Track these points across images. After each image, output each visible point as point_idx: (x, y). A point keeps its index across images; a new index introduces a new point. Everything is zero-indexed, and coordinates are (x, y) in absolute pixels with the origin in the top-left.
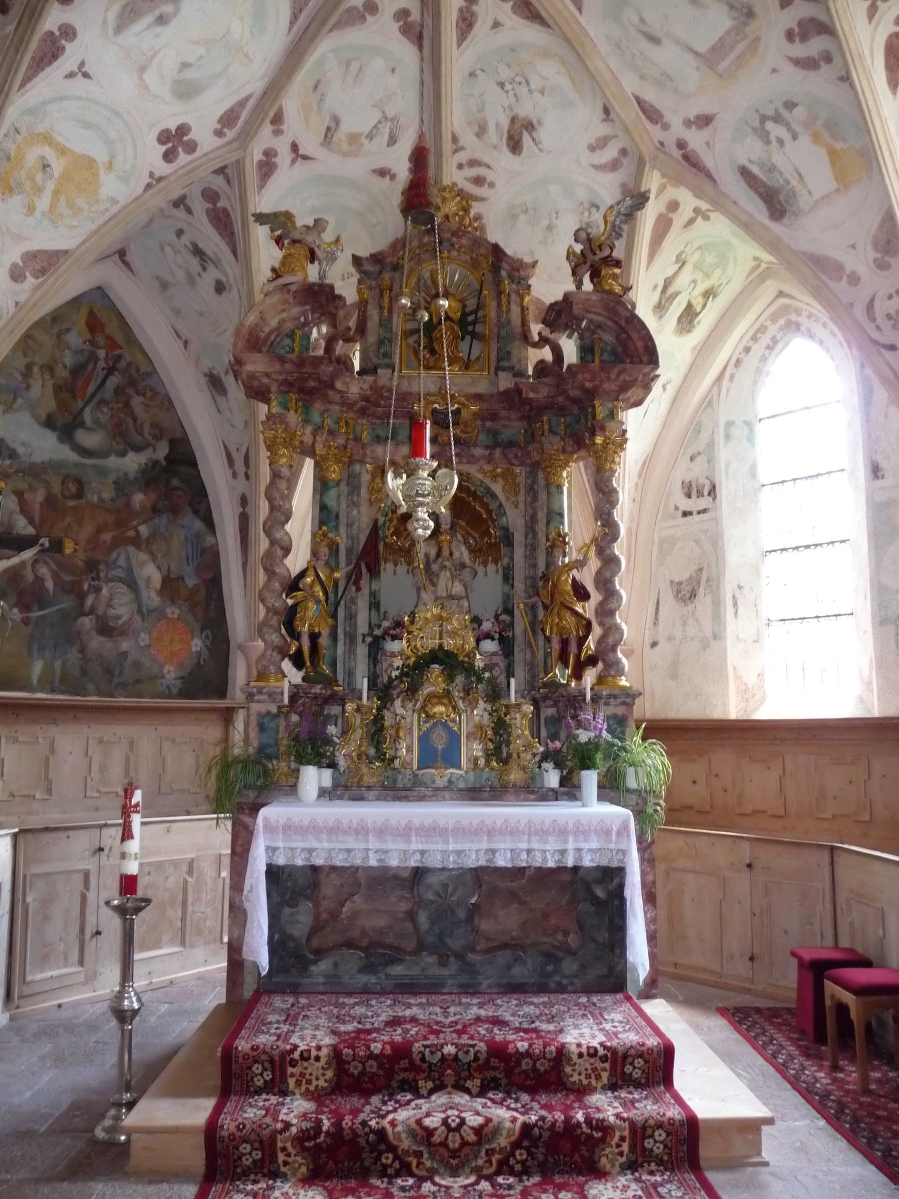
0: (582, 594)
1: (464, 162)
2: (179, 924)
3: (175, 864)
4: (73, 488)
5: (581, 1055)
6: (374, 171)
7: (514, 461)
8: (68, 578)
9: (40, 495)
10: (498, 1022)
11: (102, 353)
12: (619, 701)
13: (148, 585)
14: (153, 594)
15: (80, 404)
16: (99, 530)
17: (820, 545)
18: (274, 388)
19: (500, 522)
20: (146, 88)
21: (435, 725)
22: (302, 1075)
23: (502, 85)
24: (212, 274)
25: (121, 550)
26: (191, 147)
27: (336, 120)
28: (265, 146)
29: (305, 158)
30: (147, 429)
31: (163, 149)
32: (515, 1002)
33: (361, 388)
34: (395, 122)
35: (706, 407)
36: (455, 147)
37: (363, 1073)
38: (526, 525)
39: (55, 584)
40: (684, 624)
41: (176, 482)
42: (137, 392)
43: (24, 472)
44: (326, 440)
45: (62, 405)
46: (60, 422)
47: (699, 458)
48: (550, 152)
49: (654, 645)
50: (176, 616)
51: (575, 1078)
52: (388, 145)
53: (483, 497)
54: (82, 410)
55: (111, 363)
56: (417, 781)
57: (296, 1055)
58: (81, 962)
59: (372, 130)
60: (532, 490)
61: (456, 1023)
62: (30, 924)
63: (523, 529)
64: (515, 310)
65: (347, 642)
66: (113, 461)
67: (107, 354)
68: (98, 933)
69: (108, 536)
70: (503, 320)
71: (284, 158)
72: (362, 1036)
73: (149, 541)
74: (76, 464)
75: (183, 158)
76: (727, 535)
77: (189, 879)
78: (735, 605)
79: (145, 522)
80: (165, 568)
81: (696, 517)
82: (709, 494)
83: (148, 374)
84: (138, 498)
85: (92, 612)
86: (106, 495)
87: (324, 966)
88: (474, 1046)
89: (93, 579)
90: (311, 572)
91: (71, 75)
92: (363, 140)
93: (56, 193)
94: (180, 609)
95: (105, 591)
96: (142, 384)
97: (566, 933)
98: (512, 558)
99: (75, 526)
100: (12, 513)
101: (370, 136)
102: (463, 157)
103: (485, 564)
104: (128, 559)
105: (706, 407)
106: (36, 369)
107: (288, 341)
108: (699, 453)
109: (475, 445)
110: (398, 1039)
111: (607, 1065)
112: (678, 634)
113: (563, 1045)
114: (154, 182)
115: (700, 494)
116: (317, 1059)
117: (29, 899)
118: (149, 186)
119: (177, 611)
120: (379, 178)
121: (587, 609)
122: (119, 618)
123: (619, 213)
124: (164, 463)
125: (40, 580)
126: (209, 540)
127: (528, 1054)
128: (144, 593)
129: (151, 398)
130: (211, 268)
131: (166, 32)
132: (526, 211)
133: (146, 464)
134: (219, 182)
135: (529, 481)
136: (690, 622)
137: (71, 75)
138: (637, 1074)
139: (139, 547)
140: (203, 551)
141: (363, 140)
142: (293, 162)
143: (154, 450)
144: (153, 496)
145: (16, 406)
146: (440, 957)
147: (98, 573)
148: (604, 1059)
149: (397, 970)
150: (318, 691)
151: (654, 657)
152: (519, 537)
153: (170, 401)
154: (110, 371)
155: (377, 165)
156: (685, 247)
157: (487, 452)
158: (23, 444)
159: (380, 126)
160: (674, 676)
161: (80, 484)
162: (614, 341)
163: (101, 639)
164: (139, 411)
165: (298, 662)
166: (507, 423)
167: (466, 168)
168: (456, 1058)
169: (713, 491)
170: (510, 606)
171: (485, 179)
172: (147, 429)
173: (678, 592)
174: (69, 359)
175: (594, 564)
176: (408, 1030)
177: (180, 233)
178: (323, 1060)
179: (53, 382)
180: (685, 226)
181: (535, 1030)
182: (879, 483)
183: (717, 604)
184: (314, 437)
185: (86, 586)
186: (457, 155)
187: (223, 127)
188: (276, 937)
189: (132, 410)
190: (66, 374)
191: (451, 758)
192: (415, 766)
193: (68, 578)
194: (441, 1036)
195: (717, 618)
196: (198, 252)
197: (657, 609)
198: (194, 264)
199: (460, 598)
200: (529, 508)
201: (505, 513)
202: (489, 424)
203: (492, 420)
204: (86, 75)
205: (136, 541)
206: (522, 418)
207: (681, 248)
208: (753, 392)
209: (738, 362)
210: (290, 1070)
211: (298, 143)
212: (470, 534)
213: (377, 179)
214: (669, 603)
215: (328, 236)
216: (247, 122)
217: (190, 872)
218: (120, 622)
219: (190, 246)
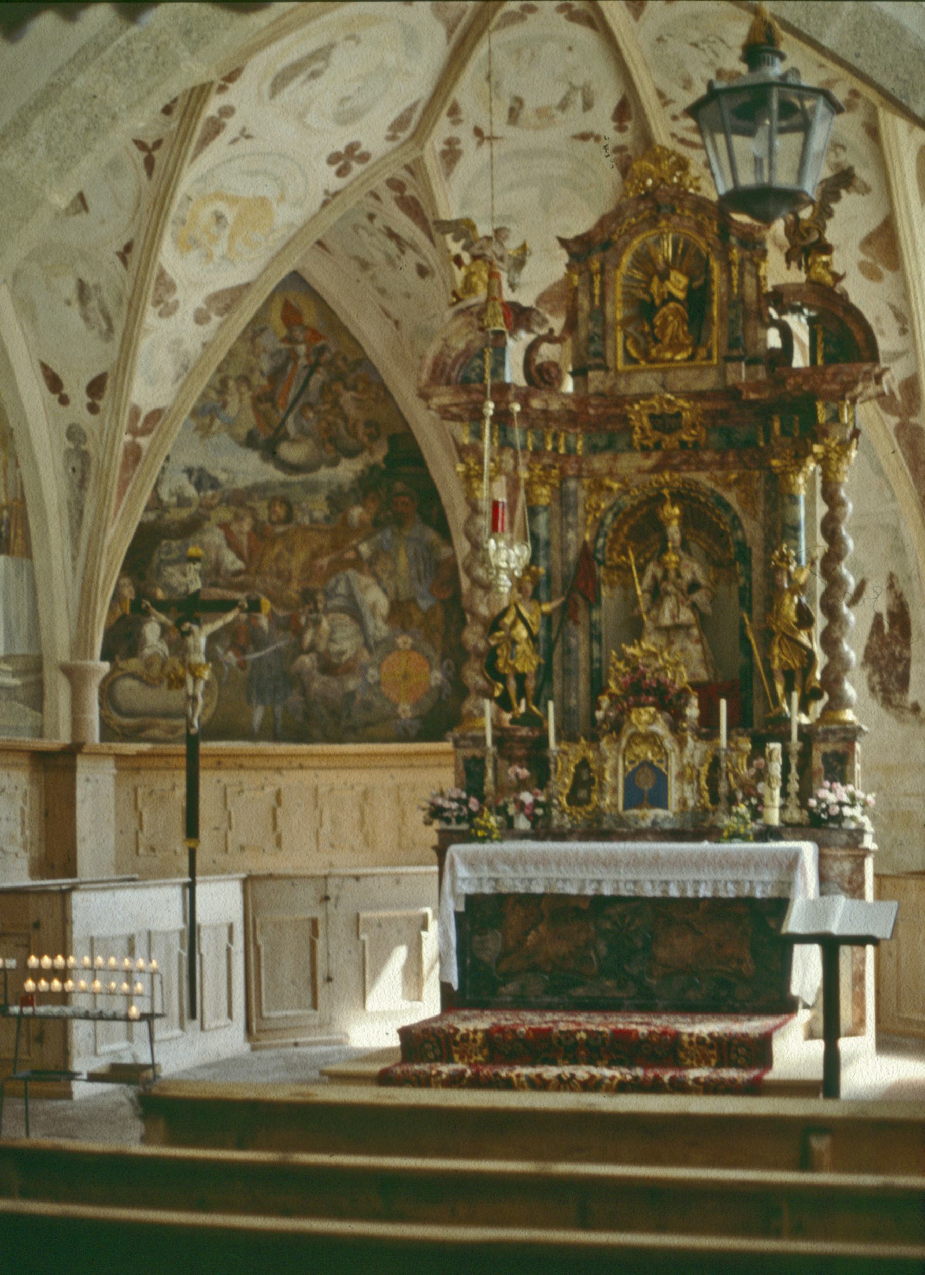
4: (280, 511)
5: (691, 1043)
6: (575, 137)
8: (281, 613)
9: (246, 525)
11: (302, 349)
13: (373, 614)
14: (380, 623)
15: (282, 412)
16: (314, 556)
20: (309, 127)
23: (696, 45)
24: (410, 260)
26: (364, 158)
30: (361, 430)
31: (334, 168)
39: (270, 622)
41: (399, 486)
42: (347, 388)
45: (261, 416)
46: (262, 438)
50: (408, 646)
54: (283, 422)
55: (313, 358)
57: (458, 1038)
62: (263, 964)
66: (324, 474)
67: (308, 349)
69: (324, 561)
71: (468, 143)
73: (372, 561)
74: (284, 484)
75: (357, 168)
80: (391, 592)
84: (356, 513)
86: (318, 515)
87: (511, 987)
89: (311, 612)
90: (513, 611)
91: (234, 141)
93: (232, 237)
95: (325, 624)
97: (740, 962)
98: (749, 578)
99: (286, 555)
100: (219, 548)
106: (231, 384)
111: (714, 1052)
114: (330, 198)
117: (260, 942)
118: (325, 204)
119: (410, 641)
122: (342, 653)
124: (383, 466)
126: (445, 552)
128: (370, 625)
130: (409, 252)
131: (319, 84)
133: (363, 471)
134: (403, 175)
137: (234, 141)
139: (360, 571)
141: (554, 111)
145: (214, 428)
147: (316, 603)
148: (711, 1047)
149: (580, 992)
154: (312, 369)
157: (718, 458)
158: (225, 470)
161: (288, 504)
163: (325, 678)
164: (351, 410)
172: (361, 430)
174: (266, 365)
175: (820, 586)
177: (371, 217)
178: (479, 1041)
179: (250, 393)
185: (303, 620)
187: (395, 131)
188: (468, 961)
189: (341, 408)
190: (264, 382)
191: (659, 799)
193: (281, 613)
196: (392, 235)
198: (392, 246)
202: (720, 422)
204: (248, 137)
205: (357, 563)
211: (481, 127)
213: (579, 143)
215: (512, 246)
218: (344, 658)
219: (384, 229)
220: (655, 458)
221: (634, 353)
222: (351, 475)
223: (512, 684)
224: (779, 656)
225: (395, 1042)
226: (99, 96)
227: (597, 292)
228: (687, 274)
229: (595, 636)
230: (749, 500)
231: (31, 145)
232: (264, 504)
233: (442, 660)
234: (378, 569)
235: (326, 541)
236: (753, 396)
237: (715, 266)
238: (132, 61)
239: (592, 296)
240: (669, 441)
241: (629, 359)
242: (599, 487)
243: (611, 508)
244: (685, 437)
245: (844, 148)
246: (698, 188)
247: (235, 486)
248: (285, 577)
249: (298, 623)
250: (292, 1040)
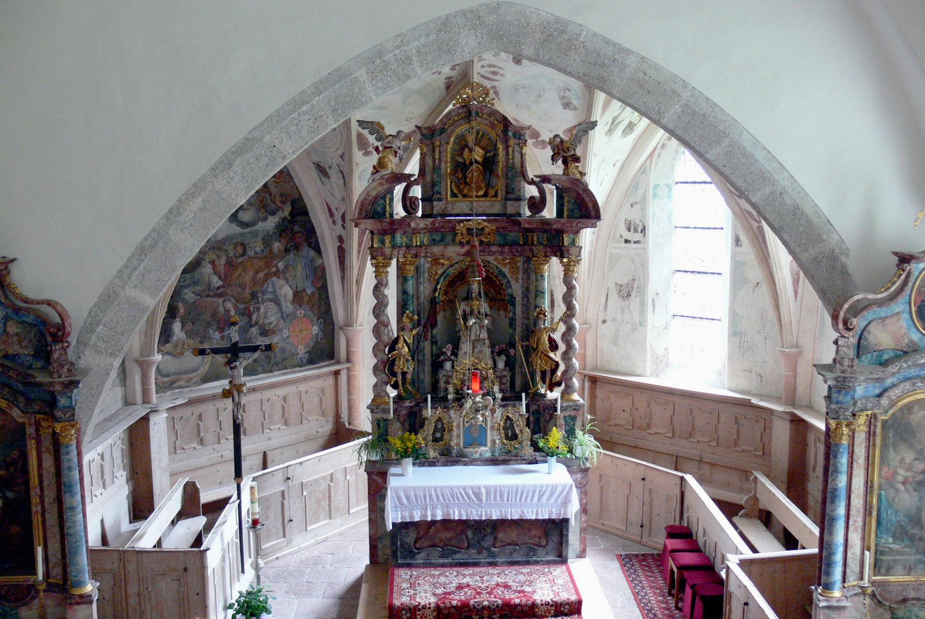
0: (554, 346)
2: (328, 508)
3: (324, 478)
4: (240, 250)
7: (516, 254)
9: (223, 261)
10: (506, 586)
14: (289, 304)
17: (706, 273)
22: (423, 614)
25: (269, 281)
30: (278, 198)
32: (514, 572)
35: (642, 173)
37: (449, 613)
38: (523, 293)
40: (623, 312)
43: (213, 248)
44: (405, 254)
47: (636, 206)
49: (604, 322)
51: (540, 613)
56: (462, 455)
57: (420, 607)
58: (284, 536)
60: (526, 271)
61: (487, 587)
64: (517, 156)
66: (260, 226)
68: (291, 520)
69: (261, 275)
70: (510, 165)
72: (447, 596)
74: (241, 234)
76: (651, 261)
77: (331, 484)
78: (654, 306)
81: (632, 244)
82: (641, 232)
84: (277, 246)
85: (256, 324)
86: (258, 249)
88: (496, 602)
89: (255, 303)
94: (305, 310)
95: (262, 309)
98: (514, 313)
99: (243, 274)
104: (274, 287)
105: (642, 173)
107: (382, 201)
108: (637, 203)
110: (463, 598)
112: (619, 317)
113: (535, 600)
115: (636, 231)
116: (429, 608)
119: (303, 312)
121: (556, 356)
122: (271, 323)
124: (289, 218)
125: (227, 311)
126: (319, 262)
127: (519, 605)
128: (284, 306)
132: (525, 87)
136: (627, 311)
138: (566, 611)
139: (279, 278)
140: (316, 269)
143: (283, 211)
146: (478, 550)
148: (552, 606)
149: (458, 556)
150: (408, 405)
151: (603, 329)
152: (519, 300)
153: (290, 175)
157: (499, 249)
160: (615, 344)
165: (395, 386)
168: (489, 607)
169: (643, 230)
173: (620, 291)
175: (562, 328)
176: (467, 592)
178: (432, 609)
181: (523, 592)
182: (738, 249)
183: (643, 304)
193: (241, 306)
194: (482, 595)
195: (643, 313)
197: (607, 300)
201: (511, 287)
205: (277, 274)
208: (672, 165)
209: (663, 146)
210: (418, 613)
214: (614, 296)
217: (331, 480)
218: (272, 326)
221: (455, 191)
222: (273, 225)
223: (400, 377)
224: (539, 364)
226: (277, 146)
227: (437, 157)
228: (483, 148)
229: (434, 343)
230: (515, 270)
231: (232, 174)
232: (232, 247)
233: (318, 320)
235: (262, 263)
236: (527, 226)
237: (500, 146)
238: (299, 126)
239: (434, 159)
241: (454, 195)
242: (436, 261)
243: (442, 274)
244: (483, 239)
245: (569, 90)
246: (493, 104)
247: (217, 239)
248: (243, 286)
249: (249, 311)
250: (275, 557)
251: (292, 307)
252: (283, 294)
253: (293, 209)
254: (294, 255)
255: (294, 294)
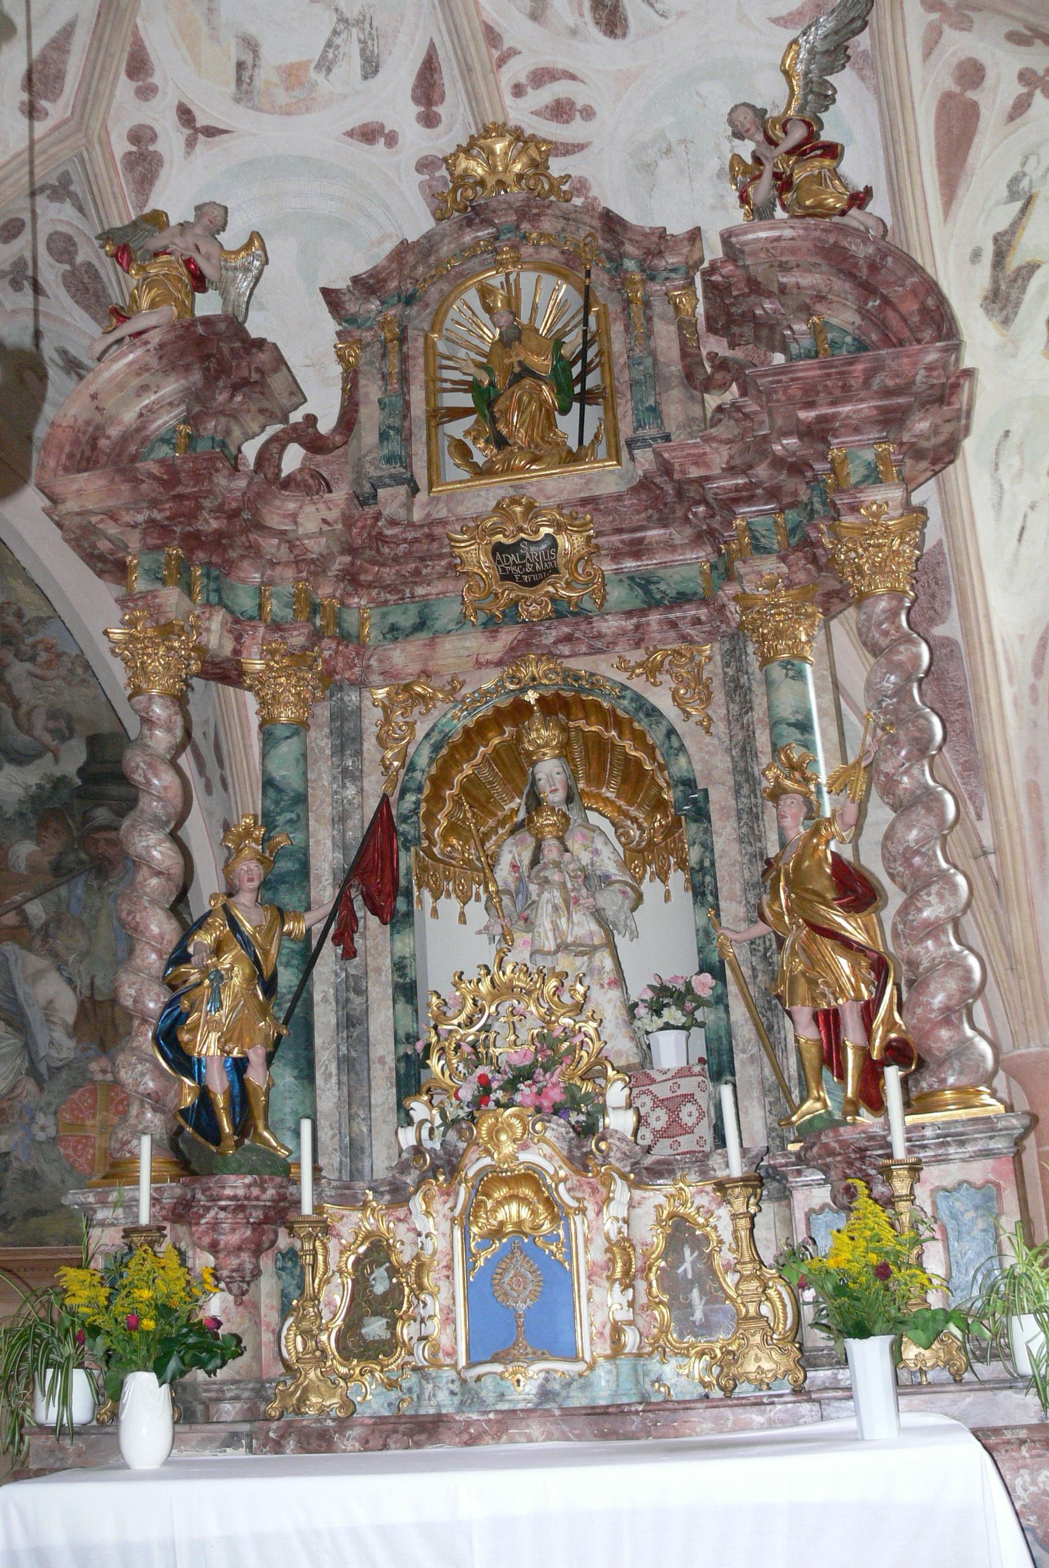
1: (523, 79)
6: (351, 134)
12: (971, 1148)
13: (48, 1020)
14: (59, 1035)
18: (134, 541)
19: (674, 770)
21: (510, 1252)
27: (251, 45)
28: (128, 124)
29: (211, 132)
30: (40, 722)
33: (325, 521)
34: (367, 26)
36: (496, 54)
48: (681, 14)
52: (365, 78)
53: (631, 721)
59: (325, 51)
63: (730, 780)
65: (344, 1078)
79: (38, 895)
80: (83, 982)
83: (41, 621)
92: (313, 74)
96: (29, 641)
101: (325, 65)
102: (517, 70)
103: (662, 875)
109: (603, 614)
120: (365, 146)
123: (812, 52)
128: (41, 1037)
129: (49, 664)
133: (40, 787)
135: (730, 671)
139: (28, 947)
141: (313, 74)
142: (191, 143)
143: (56, 760)
144: (55, 844)
153: (87, 667)
155: (355, 121)
156: (1024, 164)
157: (630, 624)
159: (338, 41)
162: (858, 320)
164: (23, 689)
166: (669, 557)
167: (529, 89)
170: (715, 958)
171: (571, 104)
172: (40, 722)
180: (1011, 118)
184: (238, 638)
186: (504, 68)
192: (462, 1361)
199: (590, 950)
200: (736, 729)
201: (682, 748)
202: (630, 564)
203: (637, 555)
206: (698, 539)
207: (1015, 168)
212: (626, 815)
213: (359, 148)
215: (232, 238)
216: (86, 80)
220: (507, 636)
222: (18, 792)
225: (967, 363)
234: (59, 944)
240: (534, 605)
251: (72, 1044)
252: (42, 1002)
253: (92, 757)
254: (89, 888)
255: (82, 1005)
